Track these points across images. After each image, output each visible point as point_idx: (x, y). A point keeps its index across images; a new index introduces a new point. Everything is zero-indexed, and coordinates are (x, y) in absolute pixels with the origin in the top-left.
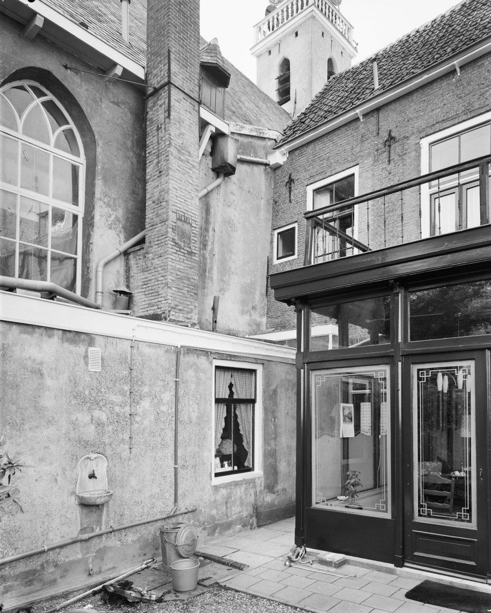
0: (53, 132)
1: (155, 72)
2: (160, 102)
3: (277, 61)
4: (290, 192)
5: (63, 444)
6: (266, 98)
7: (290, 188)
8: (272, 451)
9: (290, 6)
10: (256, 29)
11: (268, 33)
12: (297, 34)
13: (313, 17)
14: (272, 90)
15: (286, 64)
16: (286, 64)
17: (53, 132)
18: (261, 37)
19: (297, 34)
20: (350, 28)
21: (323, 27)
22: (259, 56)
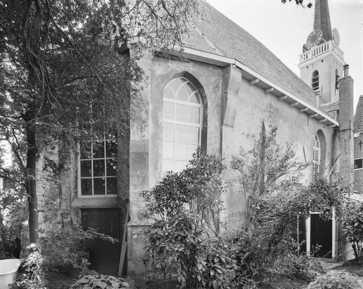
0: (189, 95)
1: (344, 125)
2: (346, 134)
3: (311, 71)
4: (361, 147)
5: (233, 249)
6: (305, 85)
7: (361, 146)
8: (7, 245)
9: (316, 50)
10: (300, 57)
11: (306, 60)
12: (322, 61)
13: (331, 55)
14: (310, 83)
15: (316, 73)
16: (316, 73)
17: (189, 95)
18: (303, 61)
19: (322, 61)
20: (343, 53)
21: (334, 57)
22: (301, 68)
